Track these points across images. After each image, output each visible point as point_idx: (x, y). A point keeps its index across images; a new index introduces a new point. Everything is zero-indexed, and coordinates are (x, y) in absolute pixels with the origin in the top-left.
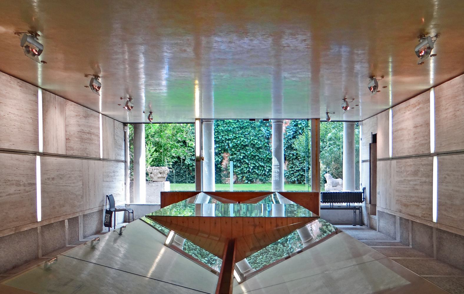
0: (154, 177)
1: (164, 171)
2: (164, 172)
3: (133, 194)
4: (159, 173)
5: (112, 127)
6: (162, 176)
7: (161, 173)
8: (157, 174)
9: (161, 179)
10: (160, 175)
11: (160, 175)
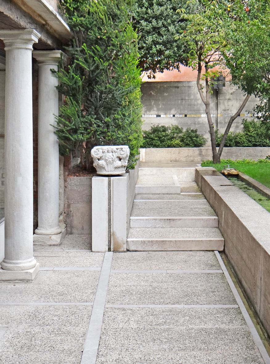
6: (123, 165)
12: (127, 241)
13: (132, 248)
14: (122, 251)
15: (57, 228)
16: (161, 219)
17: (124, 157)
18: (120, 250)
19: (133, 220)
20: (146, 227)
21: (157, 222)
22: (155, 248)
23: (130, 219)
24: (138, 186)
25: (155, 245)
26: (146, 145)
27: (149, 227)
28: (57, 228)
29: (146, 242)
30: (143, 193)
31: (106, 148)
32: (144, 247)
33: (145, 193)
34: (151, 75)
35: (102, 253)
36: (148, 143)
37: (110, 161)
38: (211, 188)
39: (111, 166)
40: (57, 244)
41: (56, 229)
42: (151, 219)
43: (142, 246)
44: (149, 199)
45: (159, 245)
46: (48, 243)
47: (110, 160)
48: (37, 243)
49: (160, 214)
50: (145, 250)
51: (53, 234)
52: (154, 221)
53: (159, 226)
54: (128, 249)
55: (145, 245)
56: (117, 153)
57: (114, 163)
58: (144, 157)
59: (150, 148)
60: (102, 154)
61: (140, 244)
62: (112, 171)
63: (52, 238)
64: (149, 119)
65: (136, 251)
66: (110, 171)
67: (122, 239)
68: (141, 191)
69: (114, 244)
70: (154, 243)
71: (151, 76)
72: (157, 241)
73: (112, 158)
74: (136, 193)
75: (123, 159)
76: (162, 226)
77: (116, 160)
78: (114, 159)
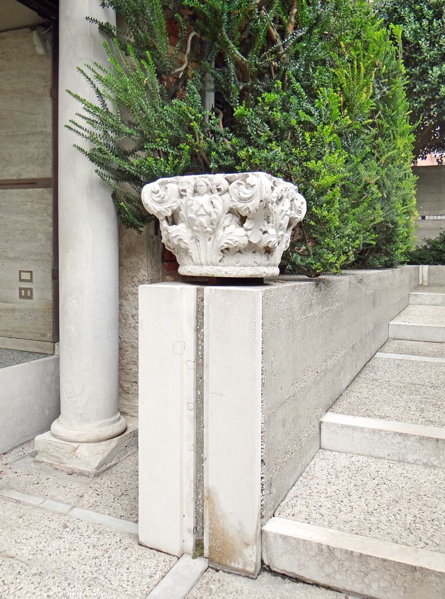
0: (193, 250)
1: (265, 206)
2: (265, 213)
3: (93, 507)
4: (228, 220)
5: (195, 580)
6: (254, 240)
7: (243, 220)
8: (215, 224)
9: (248, 258)
10: (235, 234)
11: (235, 234)
12: (262, 531)
13: (281, 564)
14: (237, 570)
15: (99, 423)
16: (422, 438)
17: (251, 209)
18: (233, 564)
19: (330, 425)
20: (372, 454)
21: (409, 443)
22: (375, 586)
23: (321, 422)
24: (394, 323)
25: (377, 576)
26: (431, 261)
27: (381, 455)
28: (99, 423)
29: (338, 554)
30: (406, 339)
31: (189, 181)
32: (328, 570)
33: (409, 338)
34: (442, 159)
35: (168, 557)
36: (433, 258)
37: (201, 225)
38: (161, 246)
39: (209, 243)
40: (89, 473)
41: (100, 426)
42: (387, 433)
43: (321, 567)
44: (413, 353)
45: (394, 578)
46: (68, 465)
47: (204, 220)
48: (44, 460)
49: (425, 414)
50: (333, 584)
51: (84, 440)
52: (398, 439)
53: (415, 457)
54: (266, 562)
55: (335, 564)
56: (227, 195)
57: (220, 232)
58: (426, 278)
59: (437, 265)
60: (179, 201)
61: (313, 554)
62: (212, 264)
63: (77, 451)
64: (437, 222)
65: (297, 580)
66: (208, 265)
67: (240, 524)
68: (401, 334)
69: (213, 536)
70: (372, 566)
71: (442, 161)
72: (385, 560)
73: (210, 214)
74: (390, 336)
75: (253, 218)
76: (425, 460)
77: (227, 222)
78: (214, 216)
